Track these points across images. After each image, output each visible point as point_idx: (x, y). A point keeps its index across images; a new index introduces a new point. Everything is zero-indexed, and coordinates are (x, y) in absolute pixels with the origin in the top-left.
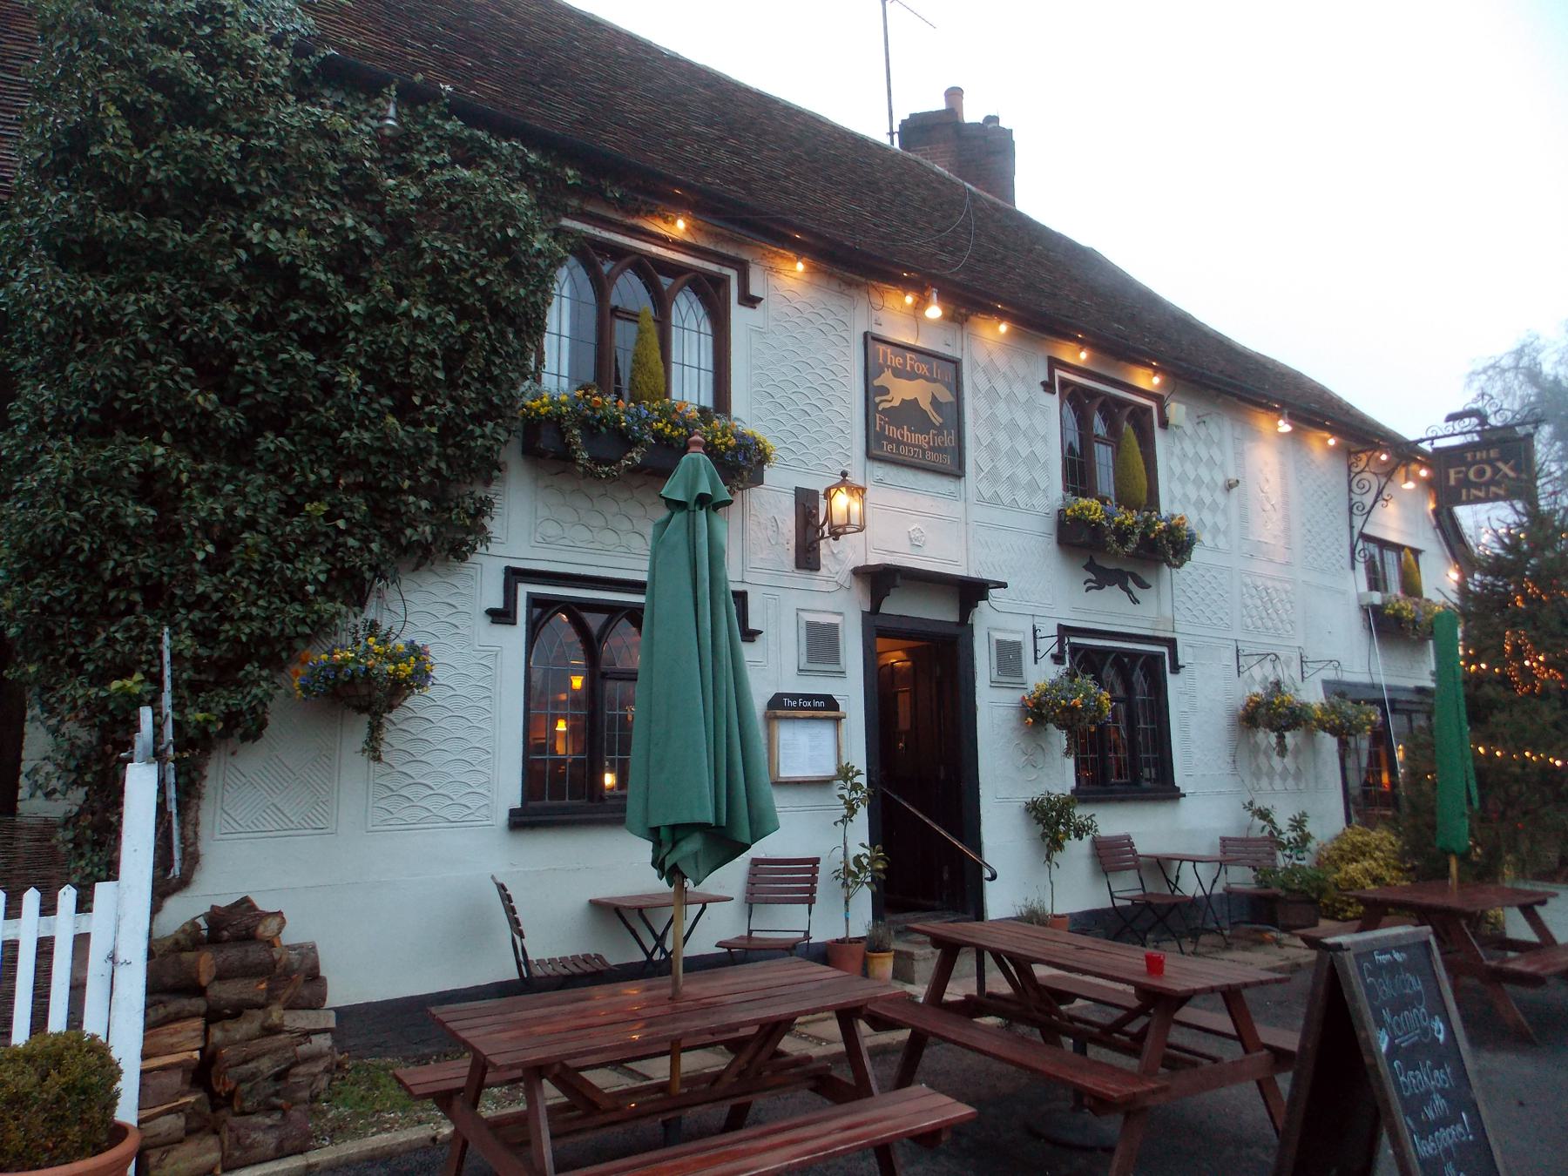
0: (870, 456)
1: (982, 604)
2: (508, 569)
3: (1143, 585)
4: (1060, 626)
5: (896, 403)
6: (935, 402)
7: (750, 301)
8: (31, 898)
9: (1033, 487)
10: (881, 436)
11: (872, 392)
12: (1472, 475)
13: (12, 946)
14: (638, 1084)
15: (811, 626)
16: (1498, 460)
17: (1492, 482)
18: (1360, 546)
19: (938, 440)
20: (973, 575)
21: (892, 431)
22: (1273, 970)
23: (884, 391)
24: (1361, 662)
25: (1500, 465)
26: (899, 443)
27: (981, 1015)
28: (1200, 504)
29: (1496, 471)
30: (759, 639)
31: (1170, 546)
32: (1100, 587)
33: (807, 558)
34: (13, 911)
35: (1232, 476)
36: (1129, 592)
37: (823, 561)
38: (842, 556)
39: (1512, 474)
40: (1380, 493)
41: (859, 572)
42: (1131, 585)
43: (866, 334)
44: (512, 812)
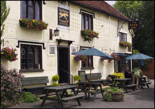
0: (58, 24)
1: (71, 44)
2: (18, 41)
3: (91, 40)
4: (80, 46)
5: (62, 17)
6: (66, 16)
7: (44, 4)
9: (78, 28)
11: (59, 15)
12: (133, 25)
14: (82, 2)
15: (51, 47)
16: (136, 23)
17: (135, 26)
18: (119, 34)
19: (66, 22)
20: (70, 40)
21: (61, 21)
22: (32, 107)
23: (60, 15)
24: (117, 49)
25: (136, 24)
26: (62, 22)
28: (98, 29)
29: (135, 25)
30: (45, 49)
31: (96, 35)
32: (85, 41)
33: (51, 38)
35: (103, 25)
36: (89, 41)
37: (53, 38)
38: (55, 38)
39: (137, 25)
40: (122, 26)
41: (57, 40)
42: (89, 40)
43: (58, 7)
44: (20, 70)
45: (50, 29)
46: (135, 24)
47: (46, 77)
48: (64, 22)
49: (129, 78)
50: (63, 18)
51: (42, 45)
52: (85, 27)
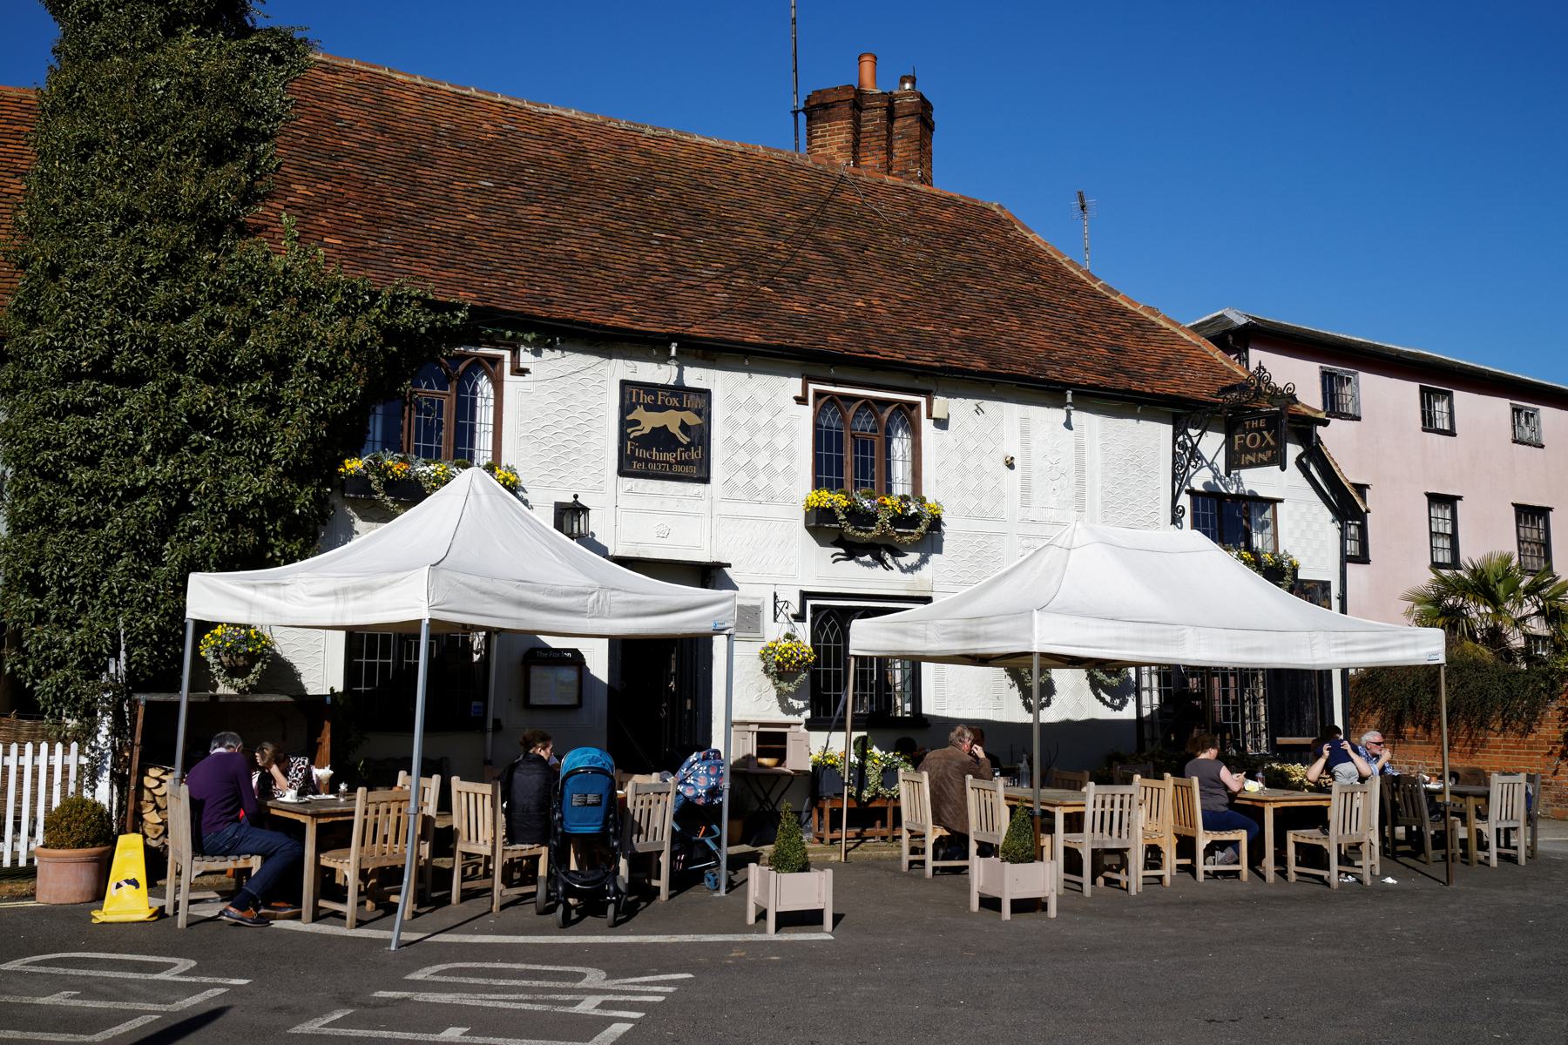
5: (647, 431)
7: (519, 371)
8: (14, 748)
10: (633, 457)
11: (625, 424)
13: (6, 769)
19: (685, 456)
27: (410, 971)
29: (1263, 438)
31: (919, 532)
34: (6, 754)
45: (556, 504)
46: (1259, 430)
47: (1038, 899)
48: (669, 457)
49: (793, 942)
50: (660, 438)
51: (809, 603)
52: (1083, 464)
